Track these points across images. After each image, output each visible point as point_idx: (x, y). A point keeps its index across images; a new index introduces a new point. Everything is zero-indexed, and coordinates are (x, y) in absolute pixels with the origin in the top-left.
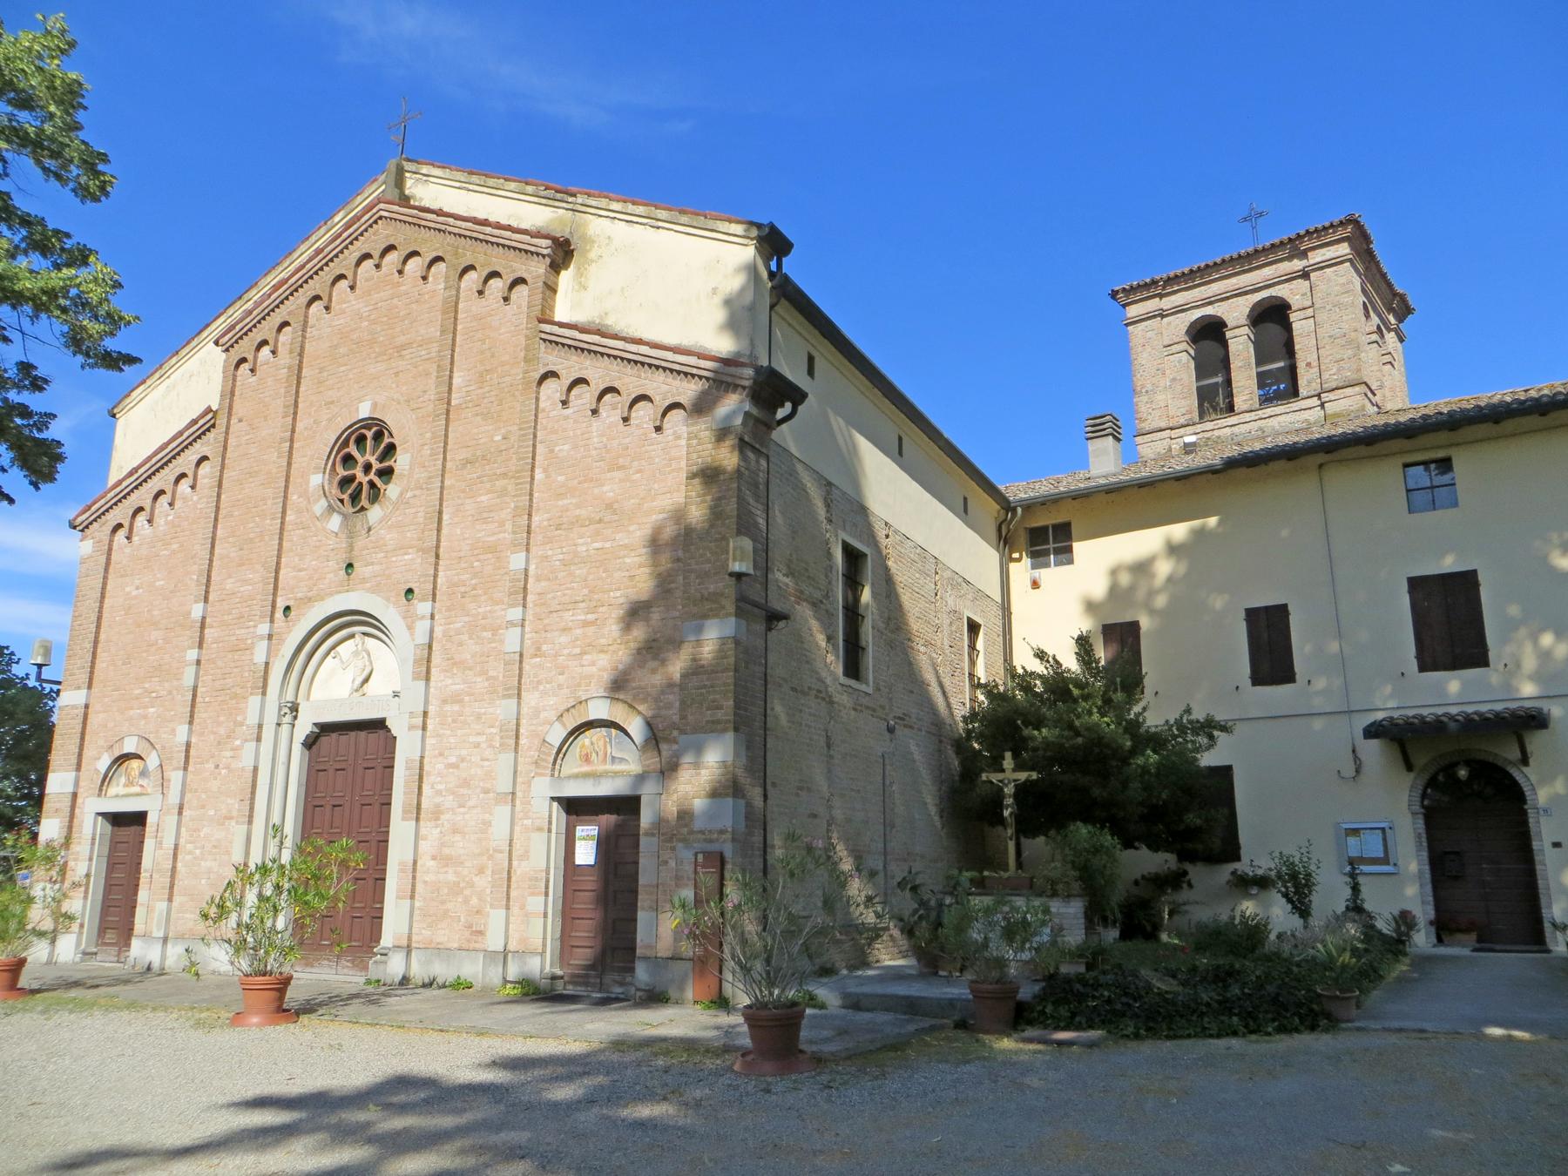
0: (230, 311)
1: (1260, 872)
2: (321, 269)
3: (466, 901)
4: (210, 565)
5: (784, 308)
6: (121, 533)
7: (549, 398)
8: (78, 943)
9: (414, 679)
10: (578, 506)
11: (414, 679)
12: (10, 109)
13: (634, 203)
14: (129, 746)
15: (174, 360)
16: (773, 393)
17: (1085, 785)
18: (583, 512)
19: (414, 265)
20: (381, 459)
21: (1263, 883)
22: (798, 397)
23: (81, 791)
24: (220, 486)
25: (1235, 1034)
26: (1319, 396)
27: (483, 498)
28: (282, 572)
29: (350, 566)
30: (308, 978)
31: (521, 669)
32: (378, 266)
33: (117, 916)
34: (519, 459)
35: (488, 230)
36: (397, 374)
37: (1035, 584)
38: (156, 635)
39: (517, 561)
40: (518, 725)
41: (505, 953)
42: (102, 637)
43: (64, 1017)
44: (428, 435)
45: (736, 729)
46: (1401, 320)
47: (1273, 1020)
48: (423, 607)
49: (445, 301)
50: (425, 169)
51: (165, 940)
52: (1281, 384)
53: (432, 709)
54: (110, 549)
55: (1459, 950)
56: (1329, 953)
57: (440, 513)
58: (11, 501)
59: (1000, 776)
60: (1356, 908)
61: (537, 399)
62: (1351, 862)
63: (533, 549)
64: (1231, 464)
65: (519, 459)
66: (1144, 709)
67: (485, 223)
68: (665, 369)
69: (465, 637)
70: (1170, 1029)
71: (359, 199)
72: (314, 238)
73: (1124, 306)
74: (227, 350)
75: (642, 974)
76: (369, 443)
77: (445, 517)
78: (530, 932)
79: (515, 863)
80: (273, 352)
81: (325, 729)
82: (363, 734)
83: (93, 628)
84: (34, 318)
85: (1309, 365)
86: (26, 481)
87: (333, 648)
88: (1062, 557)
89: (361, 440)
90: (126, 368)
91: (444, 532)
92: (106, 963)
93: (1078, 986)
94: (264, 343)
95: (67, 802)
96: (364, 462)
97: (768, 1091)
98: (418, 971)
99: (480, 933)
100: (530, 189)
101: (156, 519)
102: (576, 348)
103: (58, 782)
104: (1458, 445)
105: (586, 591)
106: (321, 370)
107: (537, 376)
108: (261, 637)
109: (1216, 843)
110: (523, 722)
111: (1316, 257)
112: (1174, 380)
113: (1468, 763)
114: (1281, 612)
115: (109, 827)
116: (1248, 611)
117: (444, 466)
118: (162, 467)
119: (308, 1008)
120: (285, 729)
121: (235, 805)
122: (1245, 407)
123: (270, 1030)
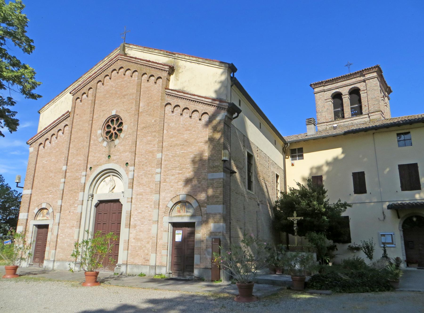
0: (74, 84)
1: (357, 246)
2: (101, 73)
3: (144, 251)
4: (68, 155)
5: (234, 87)
6: (42, 146)
7: (168, 110)
8: (27, 263)
9: (129, 188)
10: (176, 141)
11: (129, 188)
12: (7, 26)
13: (192, 57)
14: (44, 206)
15: (57, 98)
16: (233, 110)
17: (309, 220)
18: (178, 142)
19: (128, 73)
20: (118, 126)
21: (358, 249)
22: (239, 111)
23: (29, 218)
24: (71, 133)
25: (368, 291)
26: (368, 114)
27: (149, 138)
28: (89, 157)
29: (109, 156)
30: (103, 272)
31: (160, 186)
32: (118, 73)
33: (39, 253)
34: (160, 127)
35: (150, 63)
36: (123, 103)
37: (293, 165)
38: (51, 174)
39: (159, 156)
40: (159, 202)
41: (155, 266)
42: (36, 175)
43: (32, 283)
44: (133, 120)
45: (223, 204)
46: (389, 94)
47: (378, 288)
48: (131, 168)
49: (138, 83)
50: (131, 46)
51: (54, 261)
52: (358, 111)
53: (133, 197)
54: (38, 150)
55: (413, 268)
56: (392, 270)
57: (136, 142)
58: (4, 136)
59: (293, 218)
60: (385, 256)
61: (165, 110)
62: (384, 244)
63: (163, 152)
64: (346, 133)
65: (160, 127)
66: (328, 200)
67: (149, 61)
68: (202, 103)
69: (143, 177)
70: (349, 290)
71: (112, 54)
72: (99, 65)
73: (314, 89)
74: (73, 95)
75: (196, 272)
76: (115, 122)
77: (137, 143)
78: (162, 261)
79: (158, 241)
80: (87, 96)
81: (101, 202)
82: (112, 204)
83: (33, 172)
84: (13, 84)
85: (365, 106)
86: (9, 130)
87: (104, 179)
88: (300, 158)
89: (112, 121)
90: (38, 99)
91: (137, 147)
92: (36, 268)
93: (322, 278)
94: (84, 93)
95: (25, 221)
96: (113, 127)
97: (249, 307)
98: (129, 271)
99: (148, 260)
100: (162, 52)
101: (52, 142)
102: (176, 97)
103: (22, 216)
104: (412, 128)
105: (179, 164)
106: (101, 101)
107: (165, 104)
108: (83, 176)
109: (346, 238)
110: (161, 201)
111: (367, 76)
112: (327, 109)
113: (416, 216)
114: (363, 174)
115: (37, 229)
116: (353, 173)
117: (137, 129)
118: (54, 127)
119: (102, 281)
120: (90, 201)
121: (75, 223)
122: (347, 117)
123: (94, 287)
